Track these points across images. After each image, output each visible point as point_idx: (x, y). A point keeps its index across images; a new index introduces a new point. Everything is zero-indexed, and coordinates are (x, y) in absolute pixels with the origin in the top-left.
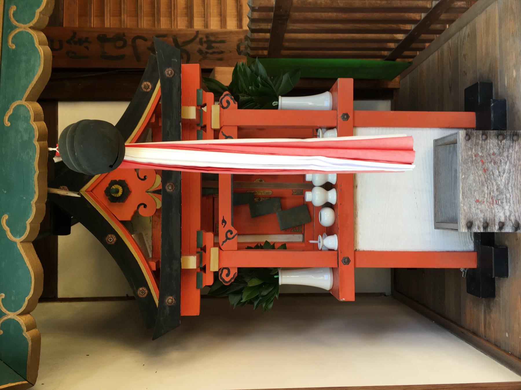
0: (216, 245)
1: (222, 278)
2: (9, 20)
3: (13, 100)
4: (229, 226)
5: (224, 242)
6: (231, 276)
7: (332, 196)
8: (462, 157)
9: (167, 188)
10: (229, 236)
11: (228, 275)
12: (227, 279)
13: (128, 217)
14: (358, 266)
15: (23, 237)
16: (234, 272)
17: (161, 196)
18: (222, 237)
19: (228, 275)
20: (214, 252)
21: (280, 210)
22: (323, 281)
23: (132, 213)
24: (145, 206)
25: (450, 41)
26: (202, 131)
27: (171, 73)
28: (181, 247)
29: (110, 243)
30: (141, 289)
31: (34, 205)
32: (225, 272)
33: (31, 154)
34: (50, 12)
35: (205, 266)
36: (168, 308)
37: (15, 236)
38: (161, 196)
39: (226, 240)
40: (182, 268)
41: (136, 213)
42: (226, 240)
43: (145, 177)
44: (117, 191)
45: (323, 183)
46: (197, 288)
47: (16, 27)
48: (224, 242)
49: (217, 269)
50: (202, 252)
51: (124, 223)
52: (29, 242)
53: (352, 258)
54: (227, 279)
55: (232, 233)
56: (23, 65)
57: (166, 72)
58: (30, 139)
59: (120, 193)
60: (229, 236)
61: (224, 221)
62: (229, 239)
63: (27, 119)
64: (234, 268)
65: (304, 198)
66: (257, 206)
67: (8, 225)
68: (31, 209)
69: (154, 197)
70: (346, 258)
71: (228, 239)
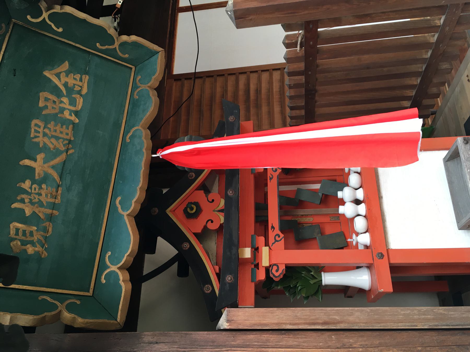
0: (267, 244)
1: (272, 273)
2: (136, 84)
3: (133, 126)
4: (277, 231)
5: (273, 244)
6: (280, 271)
7: (362, 209)
8: (464, 156)
9: (228, 192)
10: (277, 238)
11: (277, 271)
12: (277, 274)
13: (199, 230)
14: (392, 262)
15: (129, 212)
16: (282, 268)
17: (223, 214)
18: (271, 240)
19: (277, 271)
20: (265, 251)
21: (320, 235)
22: (361, 279)
23: (202, 227)
24: (212, 222)
25: (448, 104)
26: (256, 268)
27: (233, 119)
28: (238, 228)
29: (184, 249)
30: (207, 286)
31: (138, 190)
32: (275, 268)
33: (140, 157)
34: (161, 79)
35: (258, 263)
36: (228, 285)
37: (123, 211)
38: (223, 214)
39: (275, 242)
40: (240, 257)
41: (205, 227)
42: (275, 242)
43: (213, 201)
44: (192, 209)
45: (352, 199)
46: (252, 281)
47: (140, 87)
48: (273, 244)
49: (267, 265)
50: (256, 250)
51: (196, 235)
52: (132, 216)
53: (385, 254)
54: (277, 274)
55: (279, 237)
56: (141, 107)
57: (230, 119)
58: (141, 149)
59: (194, 211)
60: (277, 238)
61: (273, 227)
62: (277, 241)
63: (140, 137)
64: (278, 188)
65: (338, 211)
66: (301, 230)
67: (120, 203)
68: (137, 192)
69: (218, 214)
70: (379, 253)
71: (276, 241)
